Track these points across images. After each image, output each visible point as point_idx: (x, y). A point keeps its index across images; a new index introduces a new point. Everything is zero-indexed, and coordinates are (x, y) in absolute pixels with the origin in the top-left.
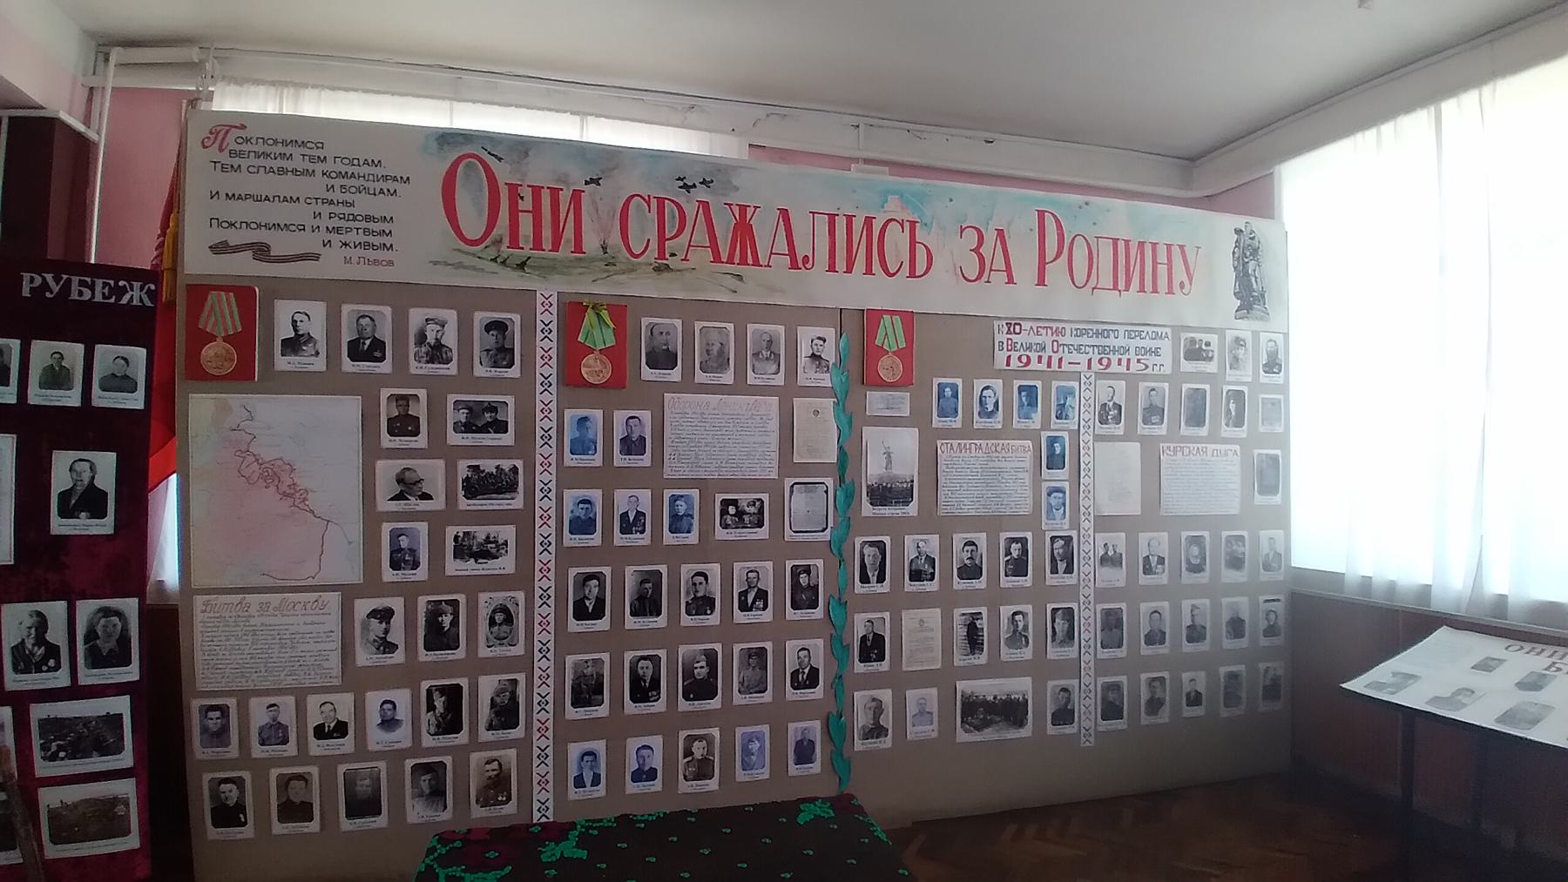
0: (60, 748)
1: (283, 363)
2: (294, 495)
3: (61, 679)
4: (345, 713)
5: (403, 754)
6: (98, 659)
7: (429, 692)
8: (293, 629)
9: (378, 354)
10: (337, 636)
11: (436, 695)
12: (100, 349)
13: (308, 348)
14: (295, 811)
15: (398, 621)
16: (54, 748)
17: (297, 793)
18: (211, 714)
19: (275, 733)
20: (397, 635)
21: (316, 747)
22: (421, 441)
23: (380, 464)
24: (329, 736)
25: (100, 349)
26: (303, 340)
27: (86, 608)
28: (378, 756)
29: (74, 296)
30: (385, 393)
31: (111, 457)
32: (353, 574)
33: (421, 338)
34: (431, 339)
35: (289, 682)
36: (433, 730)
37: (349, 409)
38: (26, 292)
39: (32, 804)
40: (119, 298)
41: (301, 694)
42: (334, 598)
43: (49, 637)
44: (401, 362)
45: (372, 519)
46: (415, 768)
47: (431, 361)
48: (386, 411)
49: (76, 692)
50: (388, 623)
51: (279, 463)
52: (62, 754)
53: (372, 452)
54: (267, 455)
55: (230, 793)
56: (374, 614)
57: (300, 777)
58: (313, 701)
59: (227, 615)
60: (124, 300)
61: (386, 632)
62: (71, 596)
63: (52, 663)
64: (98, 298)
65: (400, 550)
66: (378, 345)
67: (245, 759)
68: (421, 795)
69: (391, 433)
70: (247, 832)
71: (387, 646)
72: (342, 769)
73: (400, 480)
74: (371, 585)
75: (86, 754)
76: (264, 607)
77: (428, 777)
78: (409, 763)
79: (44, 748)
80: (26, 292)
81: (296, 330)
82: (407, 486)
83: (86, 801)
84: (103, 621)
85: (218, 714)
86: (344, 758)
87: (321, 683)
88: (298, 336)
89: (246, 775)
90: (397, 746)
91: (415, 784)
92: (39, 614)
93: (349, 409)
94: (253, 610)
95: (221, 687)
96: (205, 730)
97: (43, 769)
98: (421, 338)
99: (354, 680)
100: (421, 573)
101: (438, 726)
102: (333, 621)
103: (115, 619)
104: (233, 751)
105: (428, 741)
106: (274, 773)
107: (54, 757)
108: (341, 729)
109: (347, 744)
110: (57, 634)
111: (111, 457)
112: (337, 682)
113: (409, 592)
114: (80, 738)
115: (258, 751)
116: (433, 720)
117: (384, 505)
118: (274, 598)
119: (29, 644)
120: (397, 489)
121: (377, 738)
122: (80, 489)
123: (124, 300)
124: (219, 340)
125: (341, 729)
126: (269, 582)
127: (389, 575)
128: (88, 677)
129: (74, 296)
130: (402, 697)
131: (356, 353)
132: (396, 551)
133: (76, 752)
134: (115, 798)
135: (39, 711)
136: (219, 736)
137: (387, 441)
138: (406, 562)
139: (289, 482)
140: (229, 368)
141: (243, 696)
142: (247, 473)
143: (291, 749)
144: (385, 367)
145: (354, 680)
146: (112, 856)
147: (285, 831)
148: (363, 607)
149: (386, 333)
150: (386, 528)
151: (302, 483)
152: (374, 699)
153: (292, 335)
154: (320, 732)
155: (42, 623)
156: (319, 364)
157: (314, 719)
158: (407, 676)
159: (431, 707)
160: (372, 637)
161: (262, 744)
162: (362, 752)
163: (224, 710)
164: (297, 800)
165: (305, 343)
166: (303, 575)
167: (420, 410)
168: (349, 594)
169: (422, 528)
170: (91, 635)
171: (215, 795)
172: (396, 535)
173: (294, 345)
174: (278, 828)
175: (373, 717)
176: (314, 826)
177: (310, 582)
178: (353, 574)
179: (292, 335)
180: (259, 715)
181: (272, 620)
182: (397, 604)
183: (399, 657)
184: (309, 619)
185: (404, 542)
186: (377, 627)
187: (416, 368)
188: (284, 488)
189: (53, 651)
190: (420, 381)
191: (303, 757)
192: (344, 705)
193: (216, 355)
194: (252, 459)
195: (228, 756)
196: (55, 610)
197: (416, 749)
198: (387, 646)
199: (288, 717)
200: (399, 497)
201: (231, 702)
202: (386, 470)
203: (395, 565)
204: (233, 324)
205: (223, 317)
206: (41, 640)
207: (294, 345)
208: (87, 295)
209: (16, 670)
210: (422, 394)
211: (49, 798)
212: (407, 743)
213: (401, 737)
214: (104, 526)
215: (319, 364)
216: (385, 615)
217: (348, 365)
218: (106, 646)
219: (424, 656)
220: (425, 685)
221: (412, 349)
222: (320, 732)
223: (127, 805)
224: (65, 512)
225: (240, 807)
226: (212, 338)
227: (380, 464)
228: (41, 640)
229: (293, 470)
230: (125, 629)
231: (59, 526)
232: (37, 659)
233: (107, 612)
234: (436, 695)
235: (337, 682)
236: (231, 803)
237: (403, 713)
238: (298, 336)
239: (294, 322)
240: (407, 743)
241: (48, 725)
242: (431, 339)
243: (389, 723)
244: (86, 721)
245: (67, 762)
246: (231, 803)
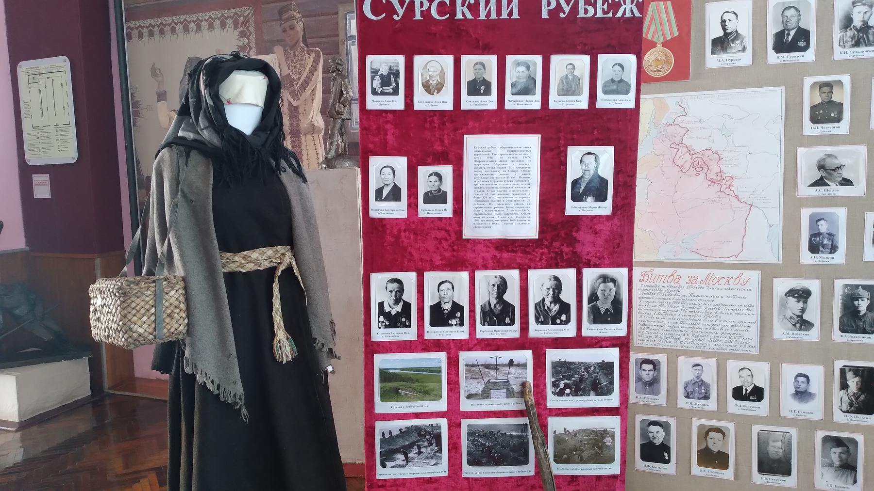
0: (567, 386)
1: (714, 61)
2: (721, 182)
3: (569, 331)
4: (762, 381)
5: (814, 425)
6: (598, 317)
7: (843, 372)
8: (717, 301)
9: (802, 44)
10: (756, 310)
11: (849, 375)
12: (602, 58)
13: (736, 45)
14: (713, 458)
15: (814, 301)
16: (562, 386)
17: (715, 443)
18: (645, 366)
19: (699, 389)
20: (813, 314)
21: (735, 406)
22: (843, 127)
23: (802, 152)
24: (746, 398)
25: (602, 58)
26: (731, 37)
27: (590, 274)
28: (791, 422)
29: (581, 14)
30: (808, 81)
31: (611, 150)
32: (772, 255)
33: (848, 22)
34: (857, 22)
35: (712, 346)
36: (845, 407)
37: (773, 99)
38: (545, 15)
39: (544, 427)
40: (615, 13)
41: (722, 359)
42: (754, 276)
43: (563, 297)
44: (825, 49)
45: (792, 203)
46: (826, 439)
47: (857, 44)
48: (810, 98)
49: (579, 342)
50: (805, 302)
51: (709, 153)
52: (568, 391)
53: (793, 139)
54: (698, 146)
55: (658, 435)
56: (791, 293)
57: (718, 430)
58: (733, 366)
59: (661, 284)
60: (619, 14)
61: (803, 310)
62: (578, 263)
63: (564, 317)
64: (600, 14)
65: (819, 234)
66: (803, 34)
67: (671, 406)
68: (831, 465)
69: (814, 120)
70: (669, 469)
71: (804, 324)
72: (756, 429)
73: (821, 167)
74: (789, 265)
75: (585, 393)
76: (692, 280)
77: (838, 450)
78: (820, 435)
79: (555, 385)
80: (545, 15)
81: (724, 28)
82: (827, 173)
83: (583, 431)
84: (602, 285)
85: (650, 367)
86: (758, 420)
87: (740, 350)
88: (726, 35)
89: (672, 421)
90: (809, 417)
91: (825, 454)
92: (556, 278)
93: (773, 99)
94: (683, 282)
95: (654, 344)
96: (639, 379)
97: (553, 401)
98: (848, 22)
99: (770, 351)
100: (839, 258)
101: (851, 405)
102: (753, 297)
103: (611, 285)
104: (661, 399)
105: (839, 417)
106: (696, 423)
107: (561, 393)
108: (757, 394)
109: (761, 408)
110: (568, 295)
111: (611, 150)
112: (754, 351)
113: (827, 275)
114: (582, 379)
115: (682, 402)
116: (846, 399)
117: (805, 190)
118: (702, 273)
119: (547, 303)
120: (817, 175)
121: (790, 406)
122: (587, 177)
123: (619, 14)
124: (659, 46)
125: (757, 394)
126: (695, 258)
127: (807, 257)
128: (591, 330)
129: (581, 14)
130: (816, 373)
131: (782, 44)
132: (815, 235)
133: (578, 390)
134: (605, 431)
135: (553, 355)
136: (652, 385)
137: (809, 129)
138: (824, 246)
139: (717, 170)
140: (667, 70)
141: (673, 355)
142: (679, 162)
143: (711, 405)
144: (809, 56)
145: (770, 351)
146: (599, 478)
147: (702, 474)
148: (782, 286)
149: (810, 23)
150: (806, 213)
151: (728, 171)
152: (789, 371)
153: (721, 33)
154: (738, 393)
155: (558, 286)
156: (746, 59)
157: (733, 382)
158: (822, 353)
159: (844, 386)
160: (789, 314)
161: (687, 397)
162: (775, 416)
163: (655, 364)
164: (715, 449)
165: (733, 41)
166: (727, 253)
167: (843, 96)
168: (768, 273)
169: (841, 214)
170: (593, 297)
171: (644, 434)
172: (815, 220)
173: (722, 43)
174: (698, 470)
175: (788, 387)
176: (728, 474)
177: (733, 260)
178: (772, 255)
179: (721, 33)
180: (685, 373)
181: (696, 292)
182: (814, 285)
183: (813, 335)
184: (731, 293)
185: (823, 227)
186: (794, 305)
187: (840, 53)
188: (712, 175)
189: (565, 308)
190: (843, 66)
191: (721, 412)
192: (761, 377)
193: (657, 60)
194: (684, 150)
195: (657, 403)
196: (568, 275)
197: (827, 421)
198: (804, 324)
199: (709, 376)
200: (820, 182)
201: (662, 359)
202: (807, 159)
203: (814, 248)
204: (671, 30)
205: (661, 24)
206: (556, 299)
207: (722, 43)
208: (591, 13)
209: (537, 321)
210: (846, 79)
211: (556, 425)
212: (819, 416)
213: (814, 409)
214: (605, 208)
215: (746, 59)
216: (803, 295)
217: (773, 58)
218: (604, 306)
219: (838, 336)
220: (839, 364)
221: (837, 34)
222: (738, 393)
223: (613, 437)
224: (576, 198)
225: (665, 447)
226: (653, 45)
227: (802, 152)
228: (556, 299)
229: (720, 159)
230: (618, 294)
231: (572, 208)
232: (553, 313)
233: (605, 279)
234: (849, 375)
235: (754, 351)
236: (658, 442)
237: (816, 386)
238: (726, 35)
239: (723, 22)
240: (819, 416)
241: (562, 367)
242: (857, 22)
243: (802, 395)
244: (587, 367)
245: (571, 397)
246: (658, 442)
